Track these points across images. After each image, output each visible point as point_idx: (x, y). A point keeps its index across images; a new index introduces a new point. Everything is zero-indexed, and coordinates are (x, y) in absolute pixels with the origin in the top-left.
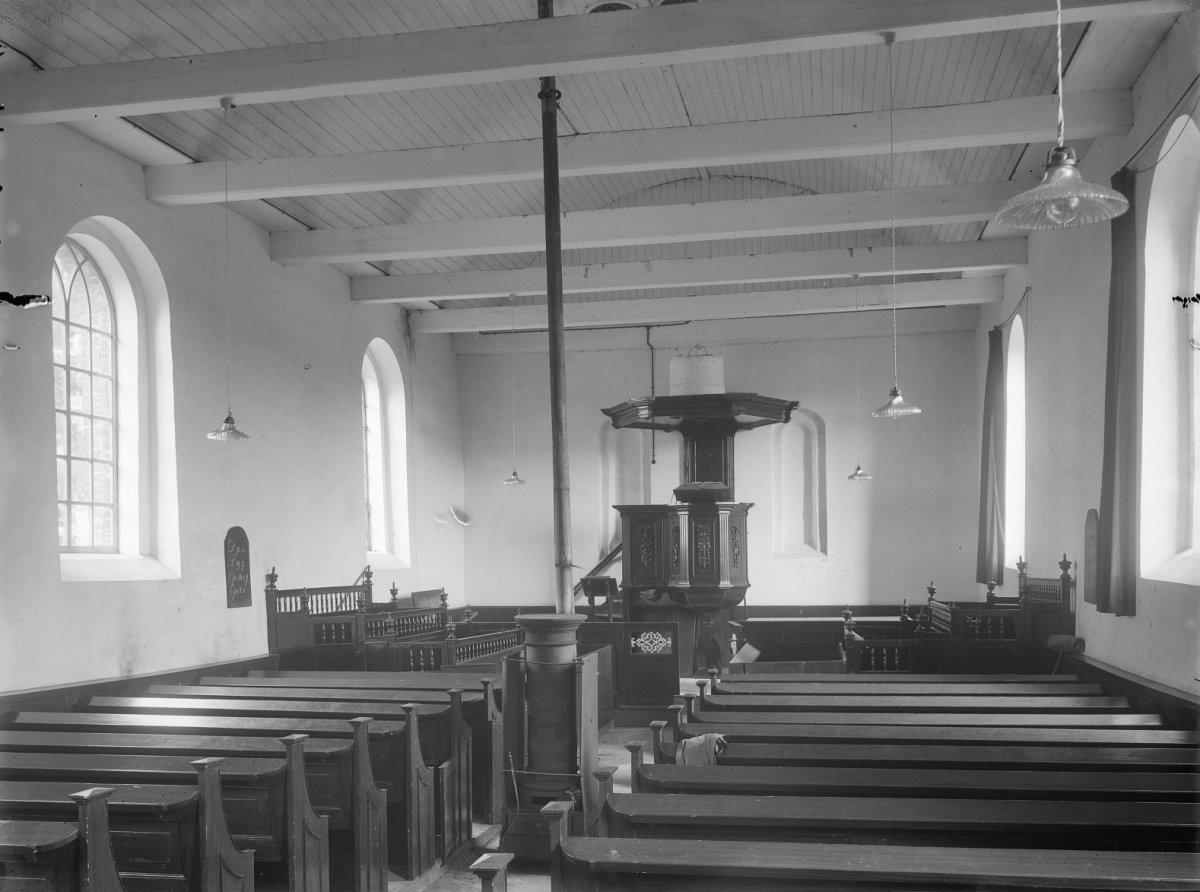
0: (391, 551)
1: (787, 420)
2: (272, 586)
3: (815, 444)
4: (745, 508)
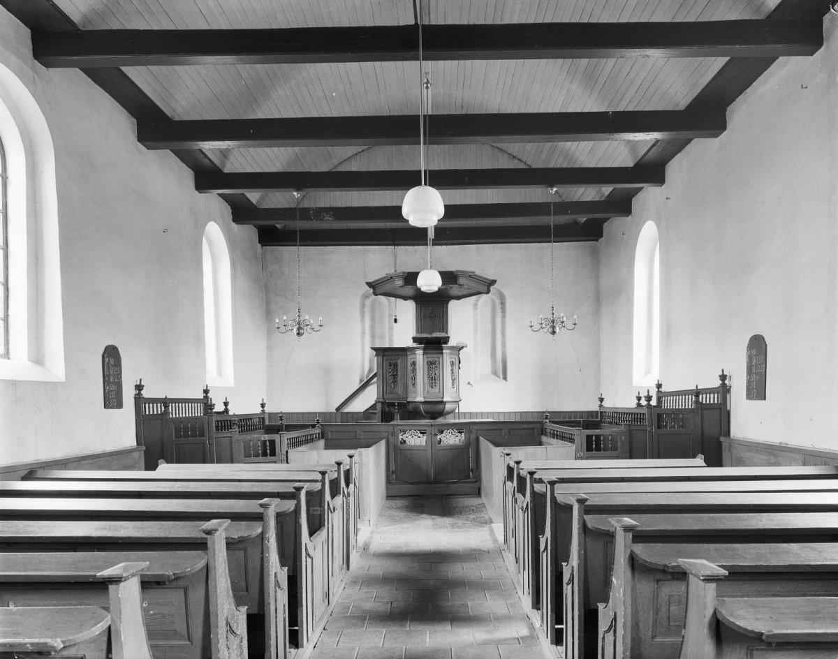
2: (139, 394)
3: (499, 319)
4: (459, 349)
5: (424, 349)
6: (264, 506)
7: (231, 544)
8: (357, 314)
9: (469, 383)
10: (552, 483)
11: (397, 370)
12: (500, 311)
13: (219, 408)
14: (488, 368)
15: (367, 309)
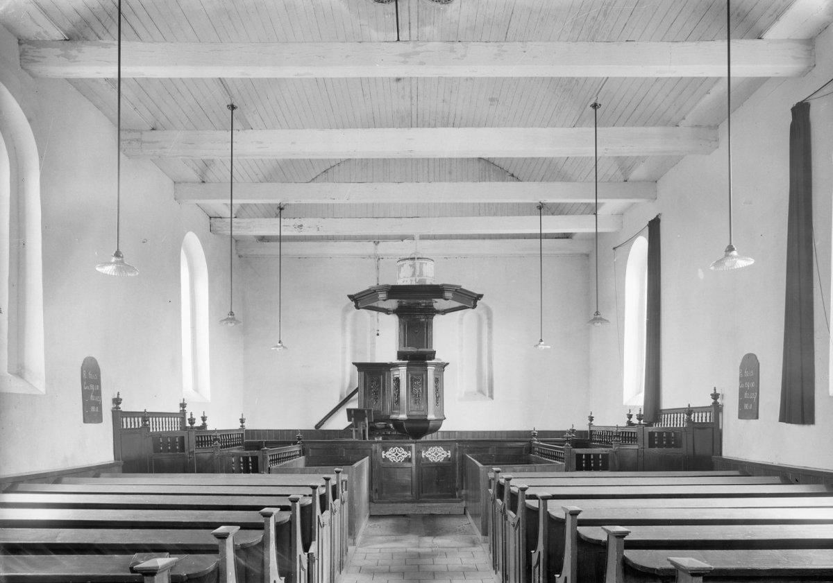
0: (196, 390)
1: (474, 307)
3: (485, 329)
5: (408, 365)
6: (223, 537)
7: (238, 550)
10: (545, 499)
13: (198, 423)
15: (348, 328)
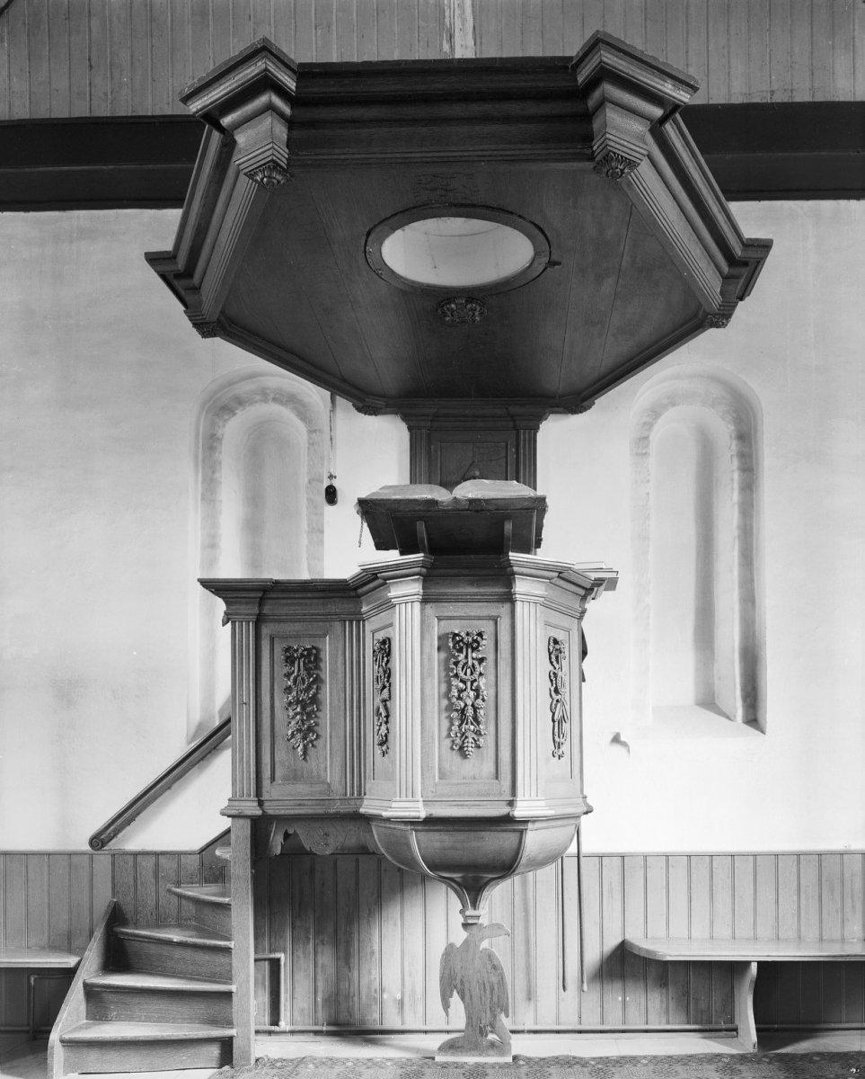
5: (429, 577)
8: (188, 476)
9: (616, 739)
11: (318, 681)
12: (736, 463)
14: (685, 686)
